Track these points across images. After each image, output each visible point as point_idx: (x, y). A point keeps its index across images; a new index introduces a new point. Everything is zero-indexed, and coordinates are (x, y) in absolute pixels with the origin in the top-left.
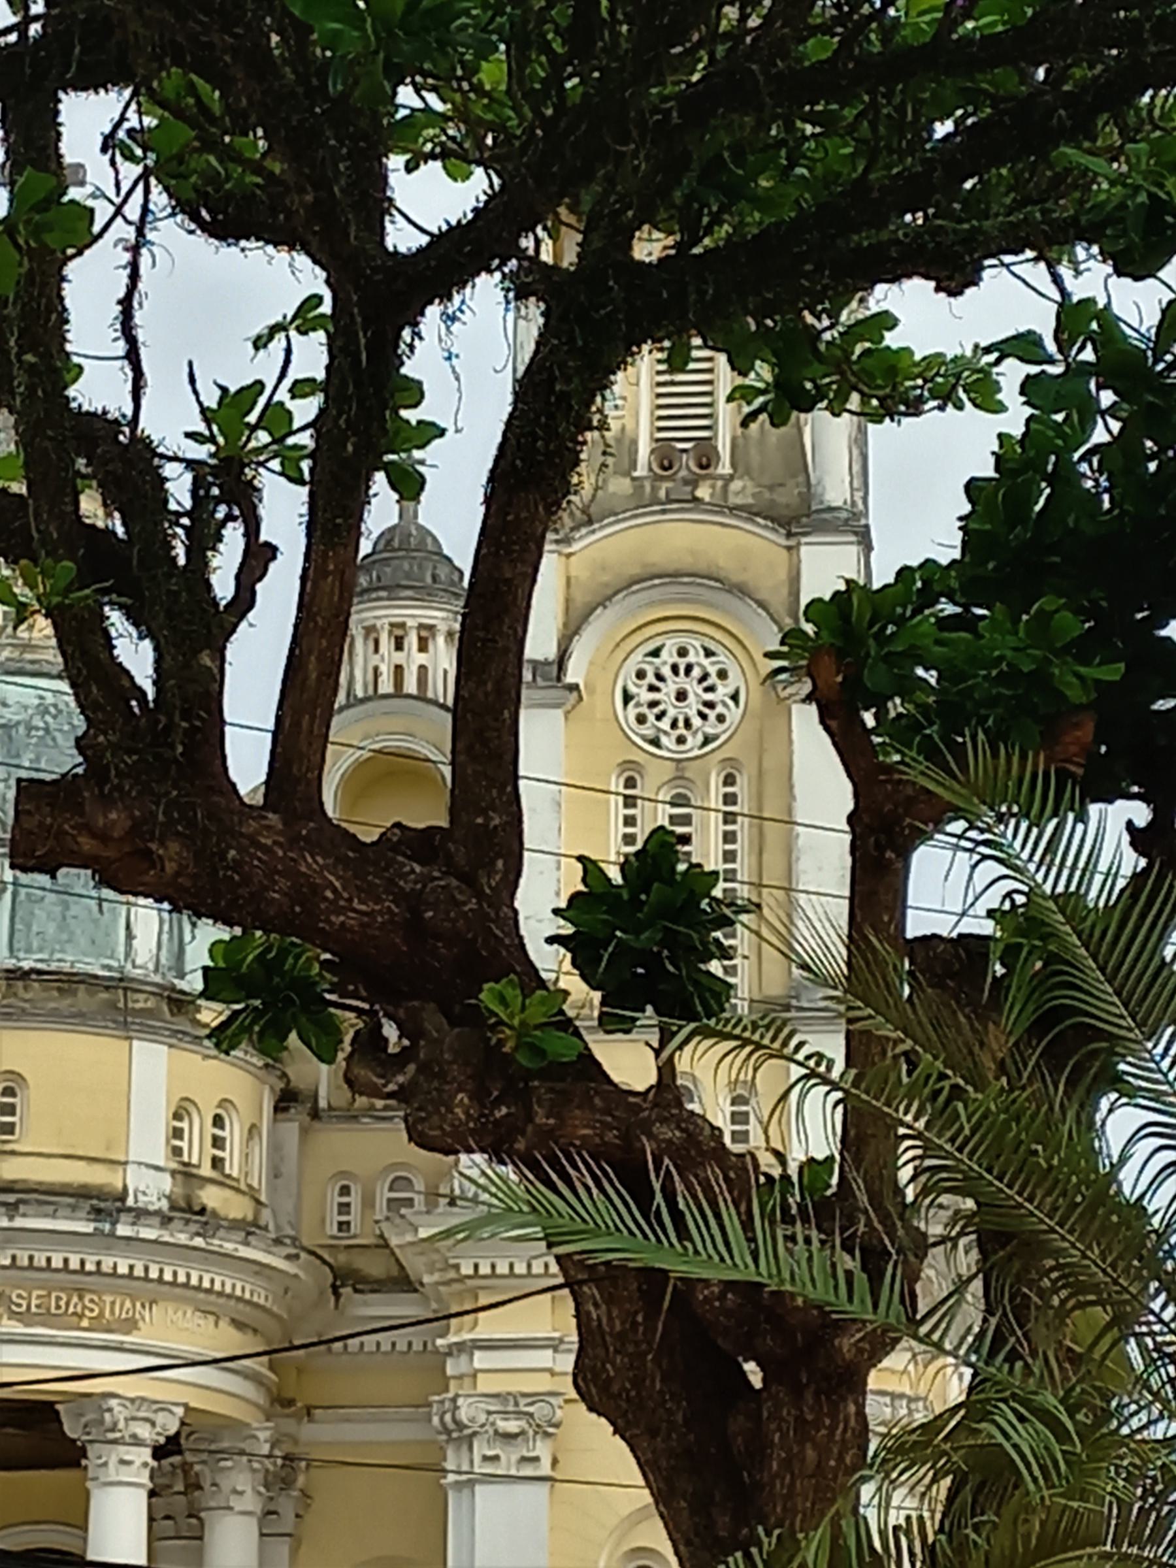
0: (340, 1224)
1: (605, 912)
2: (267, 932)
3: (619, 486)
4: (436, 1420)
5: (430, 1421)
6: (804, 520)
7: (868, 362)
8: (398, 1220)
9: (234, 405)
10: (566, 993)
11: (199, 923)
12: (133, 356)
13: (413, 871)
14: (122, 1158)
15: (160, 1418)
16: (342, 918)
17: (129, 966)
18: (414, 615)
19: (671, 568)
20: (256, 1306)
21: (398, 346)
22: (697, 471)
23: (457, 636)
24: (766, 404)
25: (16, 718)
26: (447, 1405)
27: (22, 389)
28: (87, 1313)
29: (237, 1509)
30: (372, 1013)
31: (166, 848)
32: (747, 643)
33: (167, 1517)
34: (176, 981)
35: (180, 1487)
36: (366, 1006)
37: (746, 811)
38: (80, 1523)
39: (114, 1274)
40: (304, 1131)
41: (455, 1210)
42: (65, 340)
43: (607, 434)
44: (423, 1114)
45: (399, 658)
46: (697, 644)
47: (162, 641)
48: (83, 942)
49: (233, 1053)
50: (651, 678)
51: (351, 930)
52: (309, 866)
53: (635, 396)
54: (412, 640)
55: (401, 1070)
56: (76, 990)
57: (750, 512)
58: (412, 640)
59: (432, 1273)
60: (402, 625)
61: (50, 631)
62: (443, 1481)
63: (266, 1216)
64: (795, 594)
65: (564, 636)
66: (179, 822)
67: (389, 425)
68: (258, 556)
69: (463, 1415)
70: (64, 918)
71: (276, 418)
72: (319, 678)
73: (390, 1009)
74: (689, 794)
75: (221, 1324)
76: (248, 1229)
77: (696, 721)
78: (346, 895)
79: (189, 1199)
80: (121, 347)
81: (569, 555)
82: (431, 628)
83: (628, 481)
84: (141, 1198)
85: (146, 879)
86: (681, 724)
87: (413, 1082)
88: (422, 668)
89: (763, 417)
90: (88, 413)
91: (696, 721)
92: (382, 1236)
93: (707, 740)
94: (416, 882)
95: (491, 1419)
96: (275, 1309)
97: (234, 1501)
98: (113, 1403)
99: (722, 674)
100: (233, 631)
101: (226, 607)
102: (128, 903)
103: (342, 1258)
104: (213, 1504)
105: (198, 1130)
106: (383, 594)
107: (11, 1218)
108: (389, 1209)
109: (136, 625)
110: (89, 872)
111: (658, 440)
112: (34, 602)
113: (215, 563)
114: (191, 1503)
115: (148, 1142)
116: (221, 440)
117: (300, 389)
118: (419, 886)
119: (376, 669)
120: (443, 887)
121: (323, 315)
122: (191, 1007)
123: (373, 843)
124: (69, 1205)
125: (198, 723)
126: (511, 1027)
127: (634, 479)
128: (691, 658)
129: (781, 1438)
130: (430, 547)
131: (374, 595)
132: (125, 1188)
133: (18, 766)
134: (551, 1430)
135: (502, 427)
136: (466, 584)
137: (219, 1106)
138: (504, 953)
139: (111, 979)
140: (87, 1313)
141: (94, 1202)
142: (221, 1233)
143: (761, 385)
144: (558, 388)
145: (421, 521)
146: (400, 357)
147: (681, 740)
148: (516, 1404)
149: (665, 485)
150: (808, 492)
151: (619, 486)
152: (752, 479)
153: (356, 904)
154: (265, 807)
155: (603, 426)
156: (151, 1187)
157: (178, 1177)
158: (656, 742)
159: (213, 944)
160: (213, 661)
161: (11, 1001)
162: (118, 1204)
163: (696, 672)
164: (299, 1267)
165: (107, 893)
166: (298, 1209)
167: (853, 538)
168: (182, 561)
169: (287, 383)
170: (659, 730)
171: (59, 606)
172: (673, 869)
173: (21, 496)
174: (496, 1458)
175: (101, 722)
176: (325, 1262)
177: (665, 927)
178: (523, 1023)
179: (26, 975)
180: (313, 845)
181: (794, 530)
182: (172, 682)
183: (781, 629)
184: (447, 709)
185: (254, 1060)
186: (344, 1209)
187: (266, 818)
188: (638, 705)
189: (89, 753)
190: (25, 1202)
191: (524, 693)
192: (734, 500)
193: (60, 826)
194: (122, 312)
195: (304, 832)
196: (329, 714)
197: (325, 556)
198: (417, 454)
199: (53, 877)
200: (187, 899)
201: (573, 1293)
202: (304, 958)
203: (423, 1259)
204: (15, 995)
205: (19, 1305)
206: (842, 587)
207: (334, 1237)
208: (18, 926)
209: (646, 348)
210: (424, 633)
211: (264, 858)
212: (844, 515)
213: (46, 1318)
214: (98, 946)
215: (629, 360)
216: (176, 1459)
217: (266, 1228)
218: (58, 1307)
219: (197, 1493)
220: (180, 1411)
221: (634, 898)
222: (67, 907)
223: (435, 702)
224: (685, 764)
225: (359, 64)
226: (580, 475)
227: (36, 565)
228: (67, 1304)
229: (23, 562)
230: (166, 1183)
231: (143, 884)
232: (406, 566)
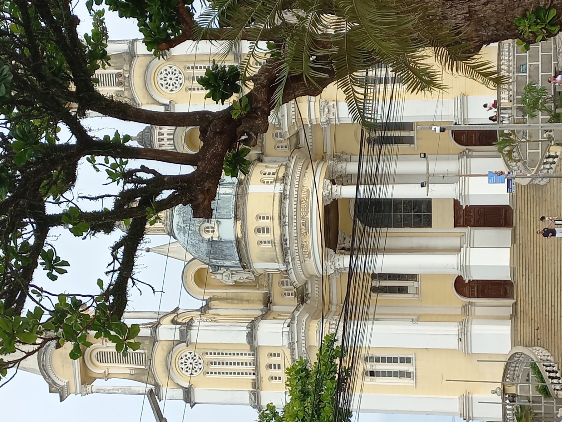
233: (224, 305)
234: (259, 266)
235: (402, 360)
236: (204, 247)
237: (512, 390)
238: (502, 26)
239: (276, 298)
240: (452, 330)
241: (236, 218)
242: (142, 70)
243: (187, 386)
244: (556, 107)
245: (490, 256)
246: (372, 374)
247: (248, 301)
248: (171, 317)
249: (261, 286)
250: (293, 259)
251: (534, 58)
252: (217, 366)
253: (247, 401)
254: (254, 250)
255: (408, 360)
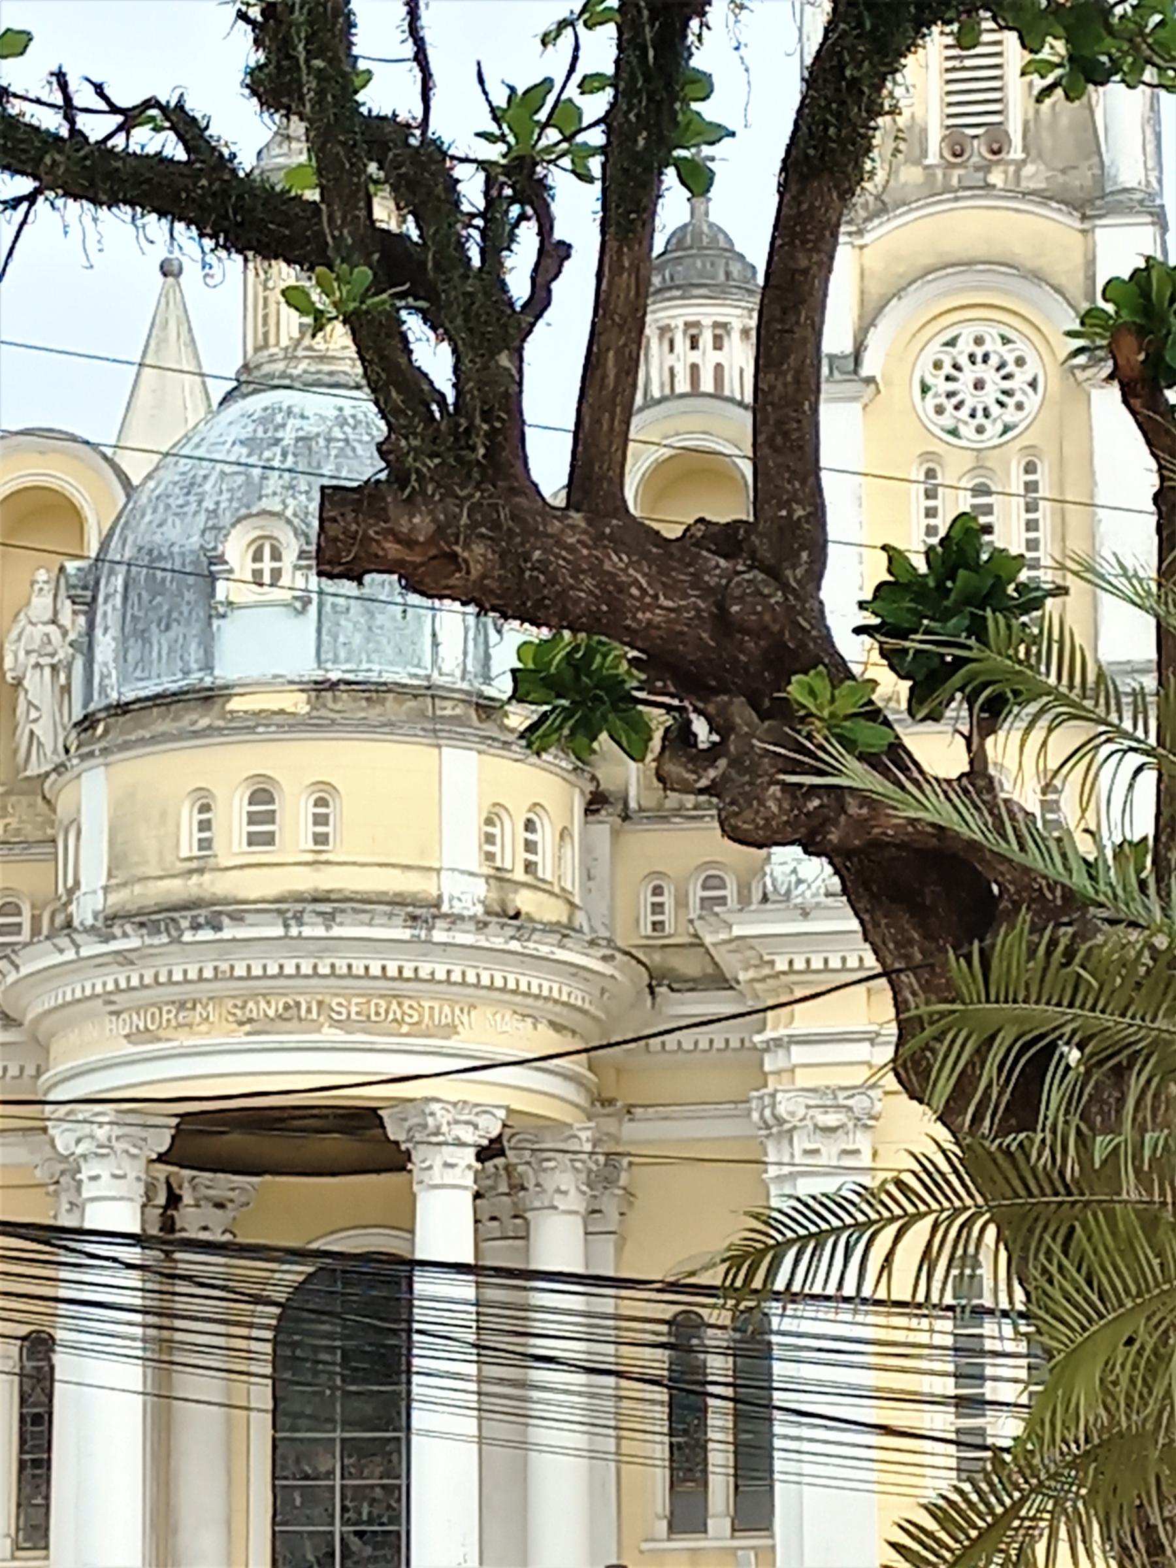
0: (654, 923)
1: (911, 600)
2: (574, 631)
3: (911, 175)
4: (755, 1116)
5: (749, 1115)
6: (1098, 203)
7: (1162, 34)
8: (712, 919)
9: (520, 111)
10: (874, 683)
11: (506, 627)
12: (421, 58)
13: (717, 566)
14: (436, 865)
15: (483, 1121)
16: (648, 615)
17: (435, 675)
18: (707, 313)
19: (965, 260)
20: (573, 1007)
21: (686, 37)
22: (990, 157)
23: (754, 333)
24: (1061, 77)
25: (315, 430)
26: (767, 1100)
27: (312, 94)
28: (407, 1019)
29: (562, 1207)
30: (681, 710)
31: (471, 551)
32: (1043, 328)
33: (493, 1218)
34: (484, 688)
35: (504, 1188)
36: (676, 702)
37: (1047, 495)
38: (408, 1227)
39: (432, 980)
40: (615, 833)
41: (769, 906)
42: (352, 44)
43: (898, 118)
44: (736, 809)
45: (694, 357)
46: (994, 332)
47: (460, 343)
48: (389, 650)
49: (544, 756)
50: (948, 369)
51: (658, 628)
52: (614, 565)
53: (924, 79)
54: (706, 339)
55: (712, 763)
56: (385, 699)
57: (1044, 197)
58: (706, 339)
59: (746, 969)
60: (697, 324)
61: (348, 341)
62: (765, 1176)
63: (580, 919)
64: (1092, 279)
65: (860, 328)
66: (482, 524)
67: (680, 117)
68: (553, 256)
69: (781, 1110)
70: (370, 628)
71: (566, 117)
72: (617, 376)
73: (700, 705)
74: (988, 482)
75: (539, 1026)
76: (564, 931)
77: (995, 410)
78: (651, 592)
79: (503, 903)
80: (409, 49)
81: (862, 247)
82: (724, 326)
83: (919, 169)
84: (455, 903)
85: (452, 582)
86: (980, 413)
87: (724, 777)
88: (719, 368)
89: (1059, 92)
90: (378, 117)
91: (995, 410)
92: (696, 936)
93: (1006, 429)
94: (720, 577)
95: (811, 1112)
96: (592, 1009)
97: (559, 1201)
98: (435, 1107)
99: (1020, 362)
100: (530, 332)
101: (524, 307)
102: (433, 609)
103: (657, 957)
104: (537, 1204)
105: (511, 834)
106: (678, 293)
107: (328, 928)
108: (702, 908)
109: (434, 328)
110: (395, 577)
111: (948, 127)
112: (331, 309)
113: (508, 264)
114: (515, 1204)
115: (461, 848)
116: (511, 139)
117: (589, 85)
118: (724, 581)
119: (672, 370)
120: (748, 581)
121: (610, 9)
122: (501, 712)
123: (678, 539)
124: (385, 913)
125: (498, 425)
126: (821, 719)
127: (927, 167)
128: (988, 347)
129: (1103, 1121)
130: (722, 243)
131: (668, 295)
132: (440, 897)
133: (322, 476)
134: (870, 1123)
135: (793, 116)
136: (761, 280)
137: (530, 810)
138: (811, 645)
139: (419, 687)
140: (407, 1019)
141: (410, 909)
142: (535, 937)
143: (1056, 59)
144: (848, 73)
145: (711, 219)
146: (689, 48)
147: (980, 430)
148: (835, 1098)
149: (956, 173)
150: (1101, 177)
151: (911, 175)
152: (1045, 163)
153: (662, 601)
154: (567, 508)
155: (894, 111)
156: (467, 893)
157: (492, 881)
158: (954, 432)
159: (525, 643)
160: (510, 361)
161: (323, 712)
162: (434, 910)
163: (994, 361)
164: (615, 967)
165: (414, 598)
166: (612, 908)
167: (1149, 219)
168: (476, 262)
169: (576, 78)
170: (959, 420)
171: (356, 312)
172: (978, 557)
173: (314, 202)
174: (816, 1152)
175: (404, 427)
176: (639, 961)
177: (972, 613)
178: (832, 715)
179: (334, 686)
180: (617, 543)
181: (1088, 213)
182: (471, 384)
183: (1077, 312)
184: (746, 407)
185: (564, 764)
186: (658, 909)
187: (568, 517)
188: (936, 395)
189: (391, 457)
190: (343, 911)
191: (824, 386)
192: (1025, 185)
193: (365, 532)
194: (408, 13)
195: (608, 530)
196: (628, 414)
197: (620, 252)
198: (706, 150)
199: (360, 583)
200: (497, 600)
201: (890, 982)
202: (610, 657)
203: (738, 956)
204: (324, 706)
205: (339, 1013)
206: (1143, 265)
207: (648, 937)
208: (325, 638)
209: (935, 29)
210: (718, 331)
211: (569, 557)
212: (1138, 196)
213: (367, 1023)
215: (920, 42)
216: (500, 1161)
217: (580, 931)
218: (377, 1014)
219: (522, 1194)
220: (502, 1114)
221: (940, 586)
222: (371, 614)
223: (731, 400)
224: (985, 453)
225: (368, 640)
226: (873, 160)
227: (332, 271)
228: (387, 1012)
229: (319, 269)
230: (480, 888)
231: (447, 587)
232: (699, 264)
234: (93, 795)
236: (183, 536)
241: (322, 688)
242: (1021, 251)
250: (124, 959)
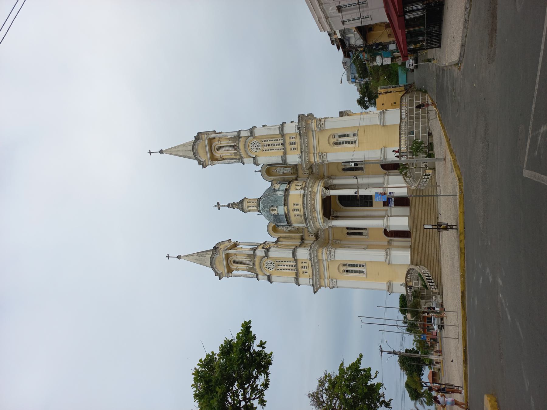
214: (282, 197)
233: (285, 240)
234: (296, 225)
235: (360, 266)
236: (272, 217)
237: (410, 284)
238: (413, 146)
239: (306, 237)
240: (382, 253)
241: (285, 205)
242: (244, 143)
243: (269, 274)
244: (429, 151)
245: (400, 221)
246: (347, 271)
247: (294, 238)
248: (262, 246)
249: (300, 232)
250: (309, 222)
251: (417, 127)
252: (281, 267)
253: (294, 281)
254: (293, 219)
255: (363, 266)
